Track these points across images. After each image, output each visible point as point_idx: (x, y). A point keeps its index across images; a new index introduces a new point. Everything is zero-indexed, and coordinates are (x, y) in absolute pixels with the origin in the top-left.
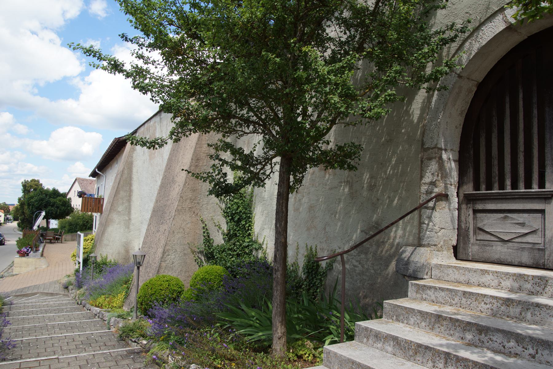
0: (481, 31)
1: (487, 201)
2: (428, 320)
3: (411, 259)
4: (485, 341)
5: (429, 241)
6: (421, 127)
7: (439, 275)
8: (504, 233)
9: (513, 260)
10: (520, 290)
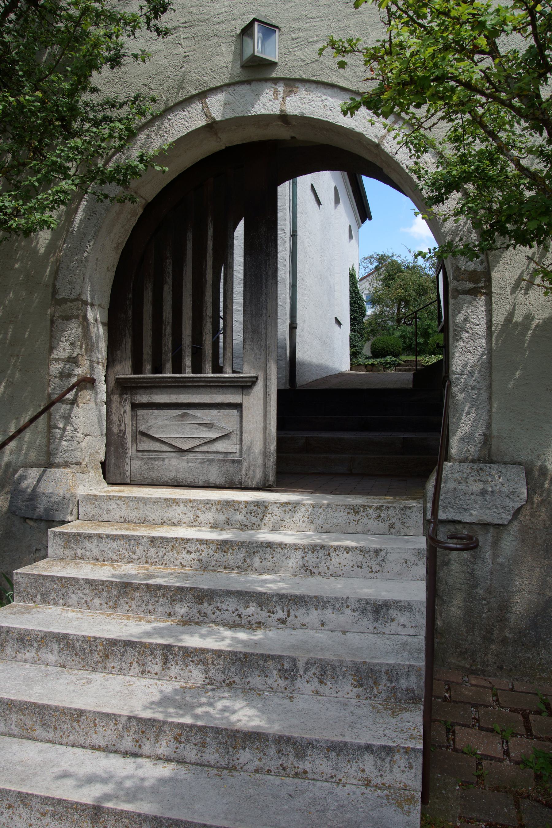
0: (167, 121)
1: (154, 390)
2: (105, 593)
3: (40, 490)
4: (209, 612)
5: (67, 457)
6: (52, 262)
7: (93, 513)
8: (181, 440)
9: (196, 480)
10: (228, 524)
